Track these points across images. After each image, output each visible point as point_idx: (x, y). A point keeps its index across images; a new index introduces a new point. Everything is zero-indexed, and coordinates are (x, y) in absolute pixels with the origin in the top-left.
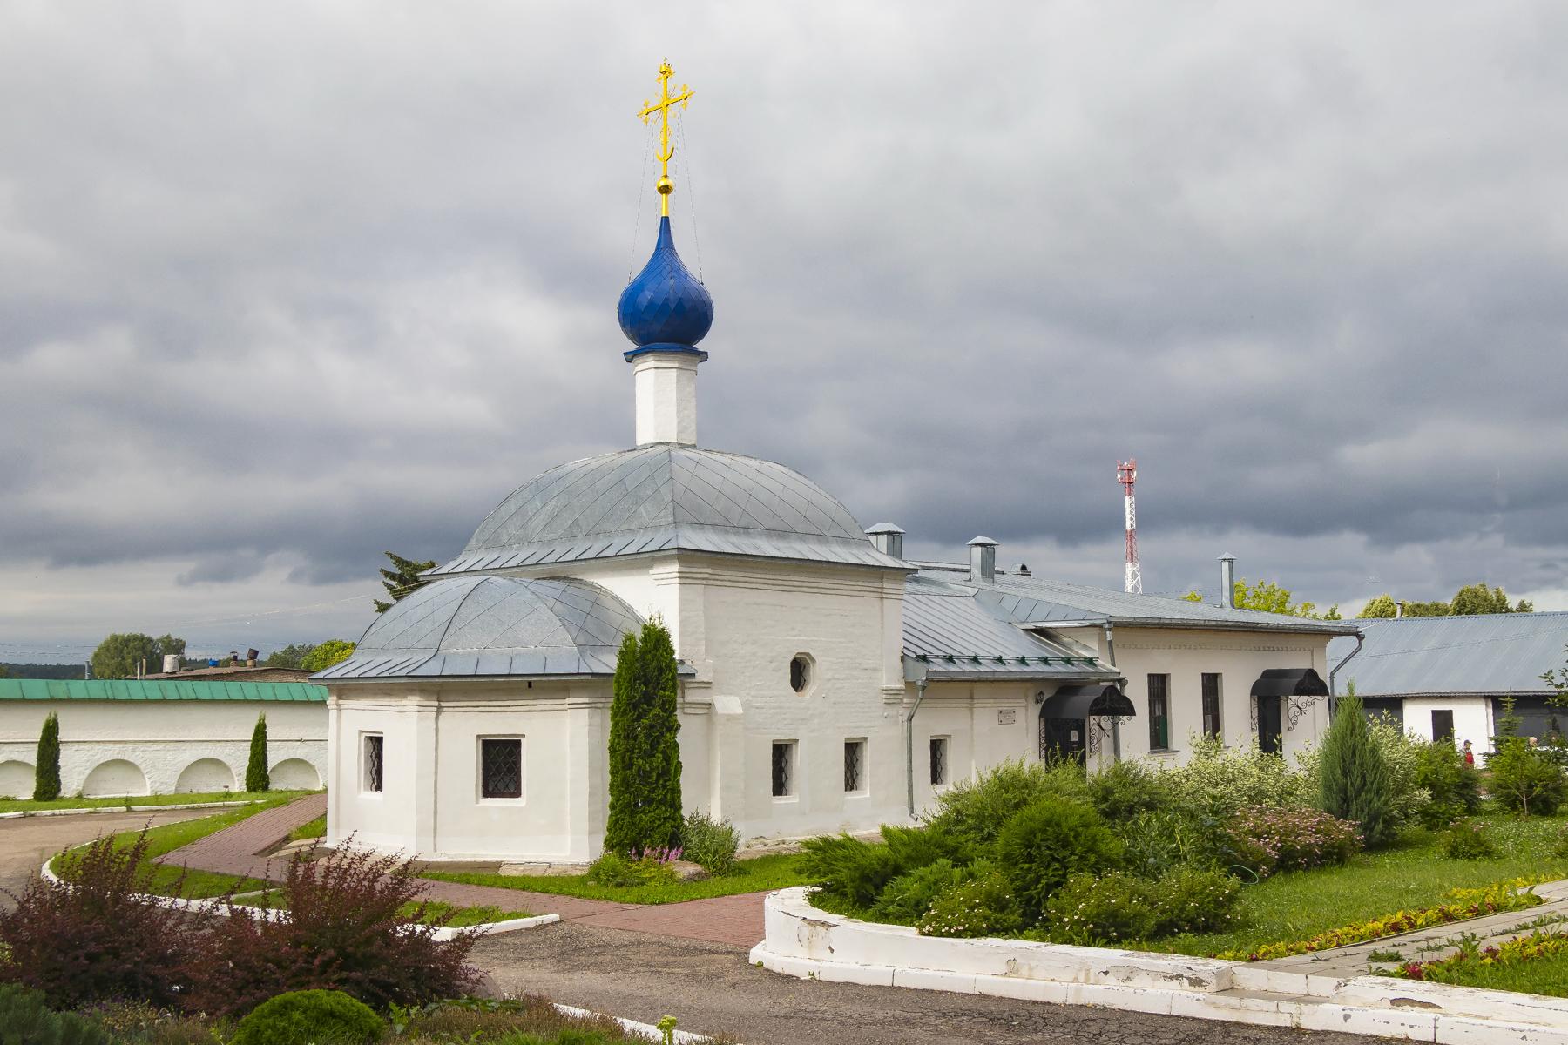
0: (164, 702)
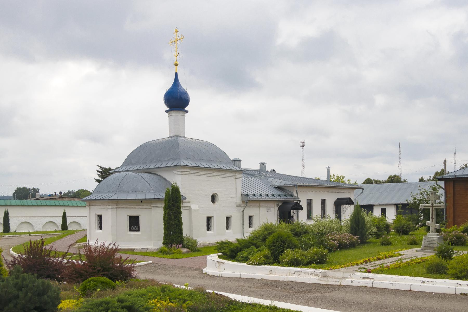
0: (37, 206)
